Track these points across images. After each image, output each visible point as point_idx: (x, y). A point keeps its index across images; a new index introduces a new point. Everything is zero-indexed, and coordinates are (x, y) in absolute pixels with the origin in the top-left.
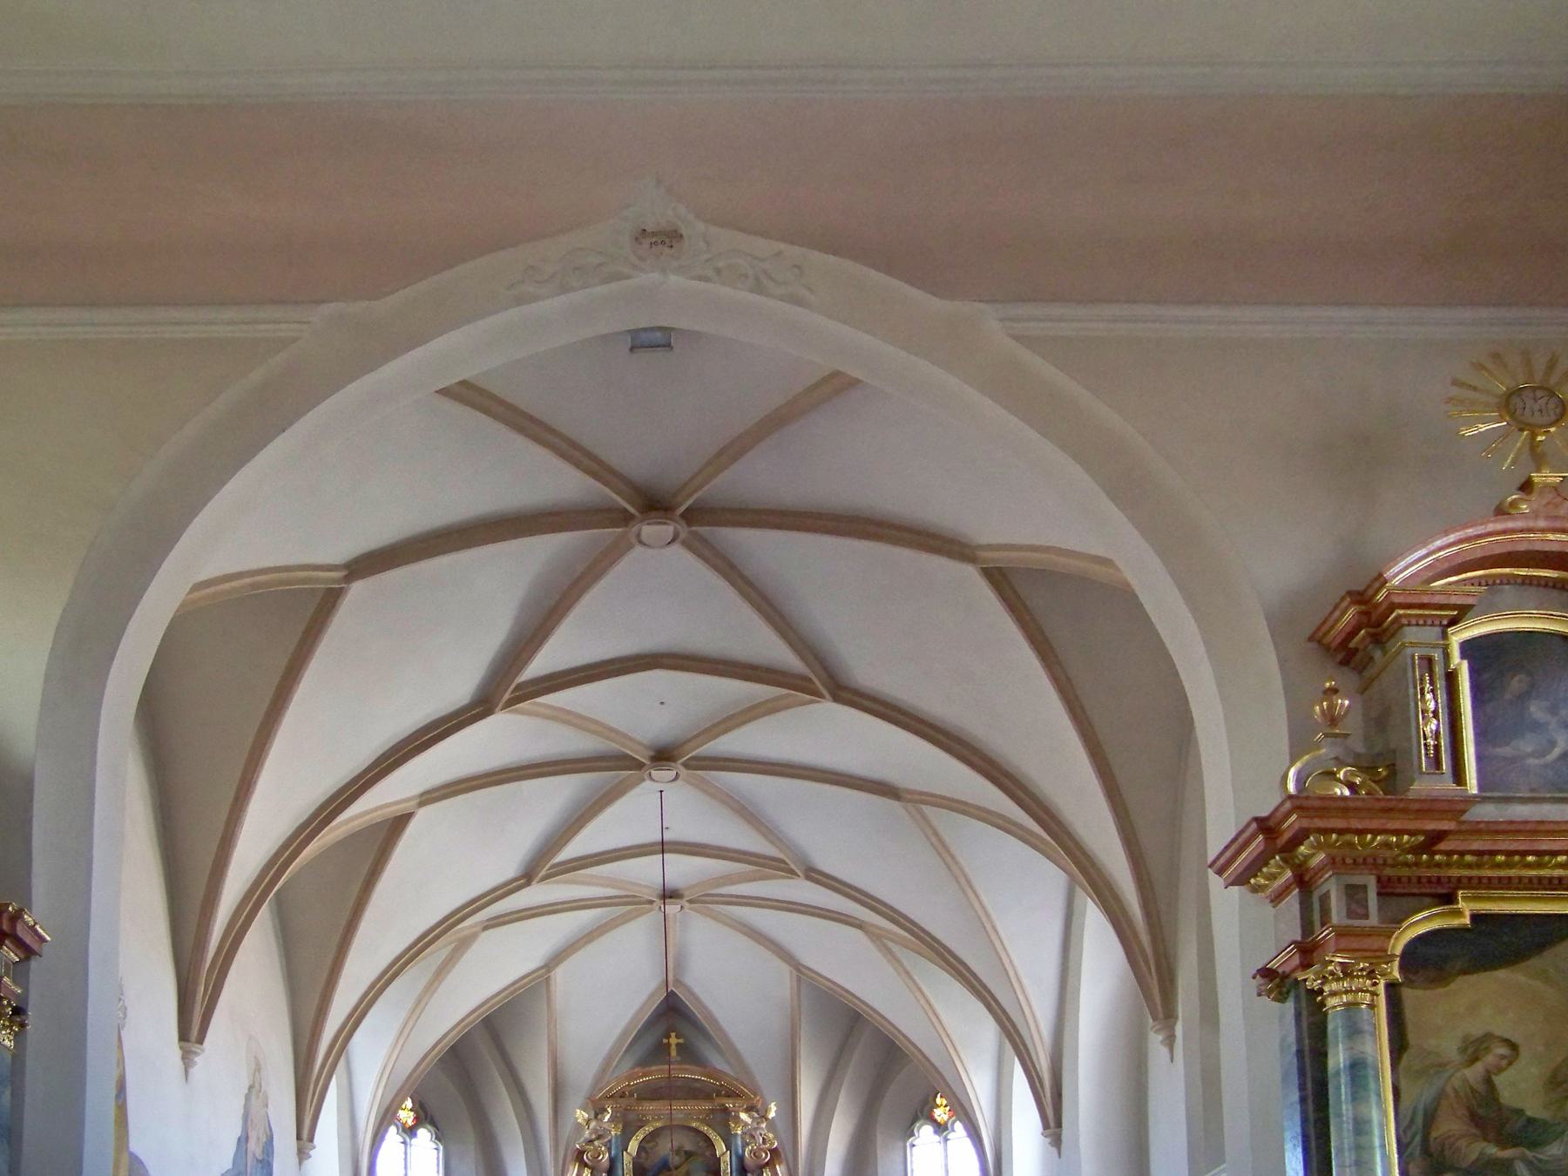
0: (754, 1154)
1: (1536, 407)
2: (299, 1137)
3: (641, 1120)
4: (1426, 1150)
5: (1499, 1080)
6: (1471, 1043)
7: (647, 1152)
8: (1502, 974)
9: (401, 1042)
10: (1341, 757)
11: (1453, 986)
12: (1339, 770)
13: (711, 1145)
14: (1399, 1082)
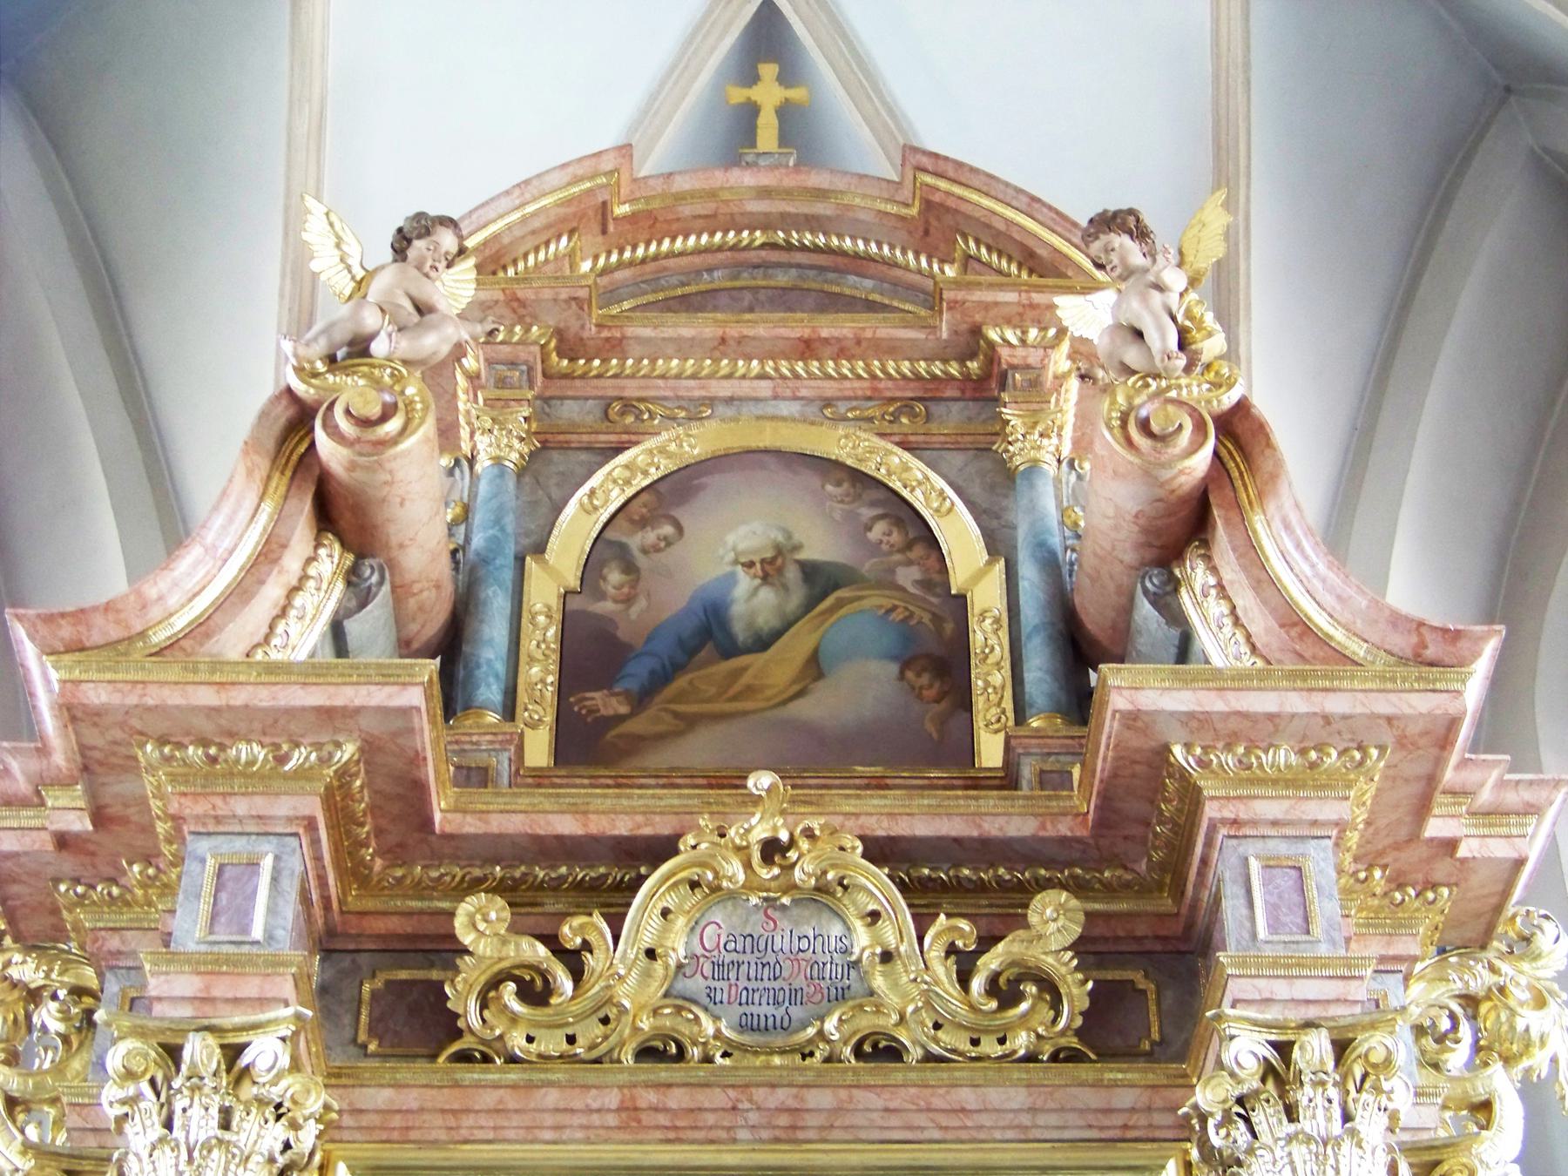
0: (1145, 426)
7: (630, 568)
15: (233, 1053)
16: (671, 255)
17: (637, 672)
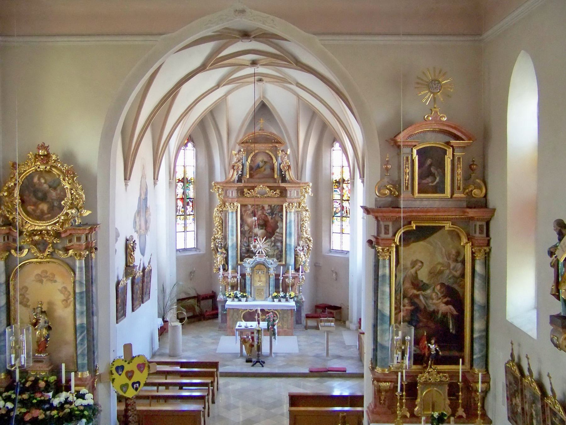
1: (435, 87)
2: (154, 179)
5: (418, 272)
9: (183, 126)
12: (388, 185)
15: (233, 204)
17: (254, 169)
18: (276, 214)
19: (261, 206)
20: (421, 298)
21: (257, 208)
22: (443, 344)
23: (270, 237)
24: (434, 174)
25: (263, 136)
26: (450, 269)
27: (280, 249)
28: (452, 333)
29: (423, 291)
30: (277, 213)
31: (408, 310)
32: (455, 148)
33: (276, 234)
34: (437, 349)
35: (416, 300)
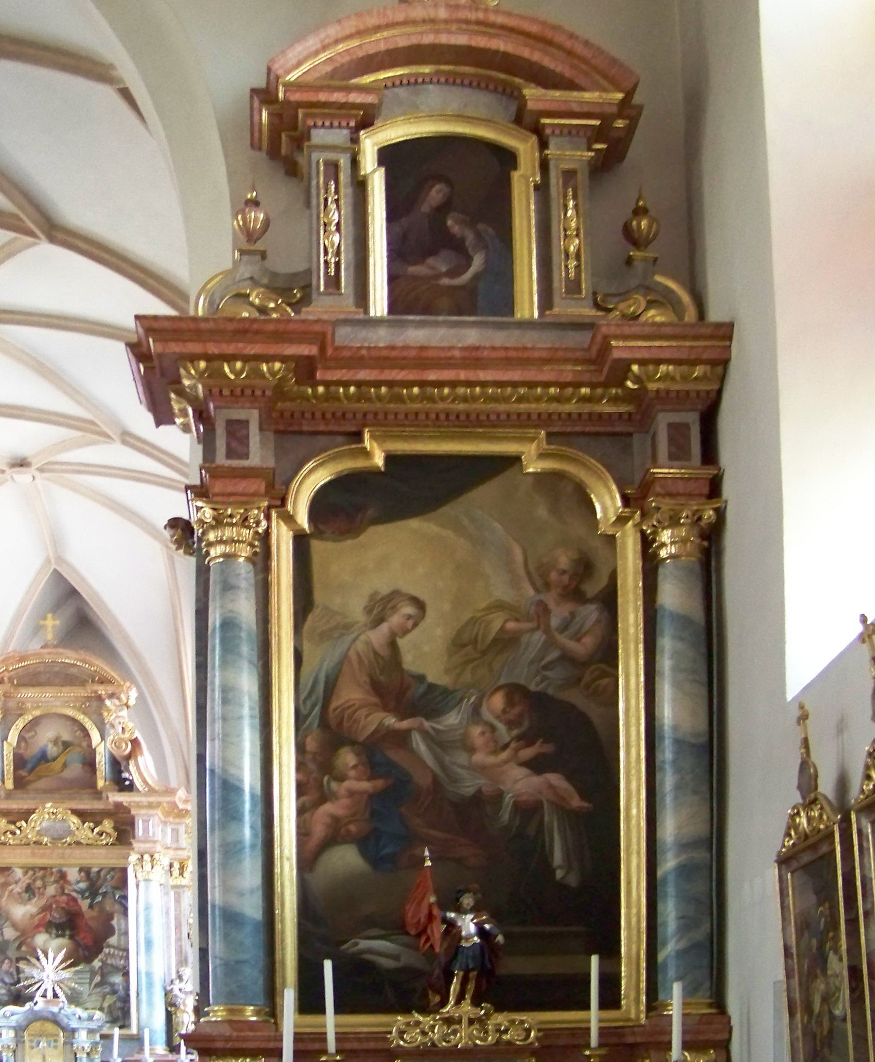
3: (21, 709)
4: (324, 723)
5: (401, 642)
6: (378, 602)
7: (26, 742)
8: (414, 523)
10: (256, 277)
11: (363, 538)
13: (87, 734)
14: (302, 646)
16: (33, 664)
17: (29, 766)
18: (104, 894)
19: (54, 870)
20: (419, 743)
21: (43, 878)
22: (517, 929)
23: (89, 960)
24: (463, 240)
25: (57, 669)
26: (547, 631)
27: (121, 992)
28: (562, 886)
29: (428, 717)
30: (110, 890)
31: (361, 793)
32: (548, 131)
33: (106, 950)
34: (487, 926)
35: (395, 755)
